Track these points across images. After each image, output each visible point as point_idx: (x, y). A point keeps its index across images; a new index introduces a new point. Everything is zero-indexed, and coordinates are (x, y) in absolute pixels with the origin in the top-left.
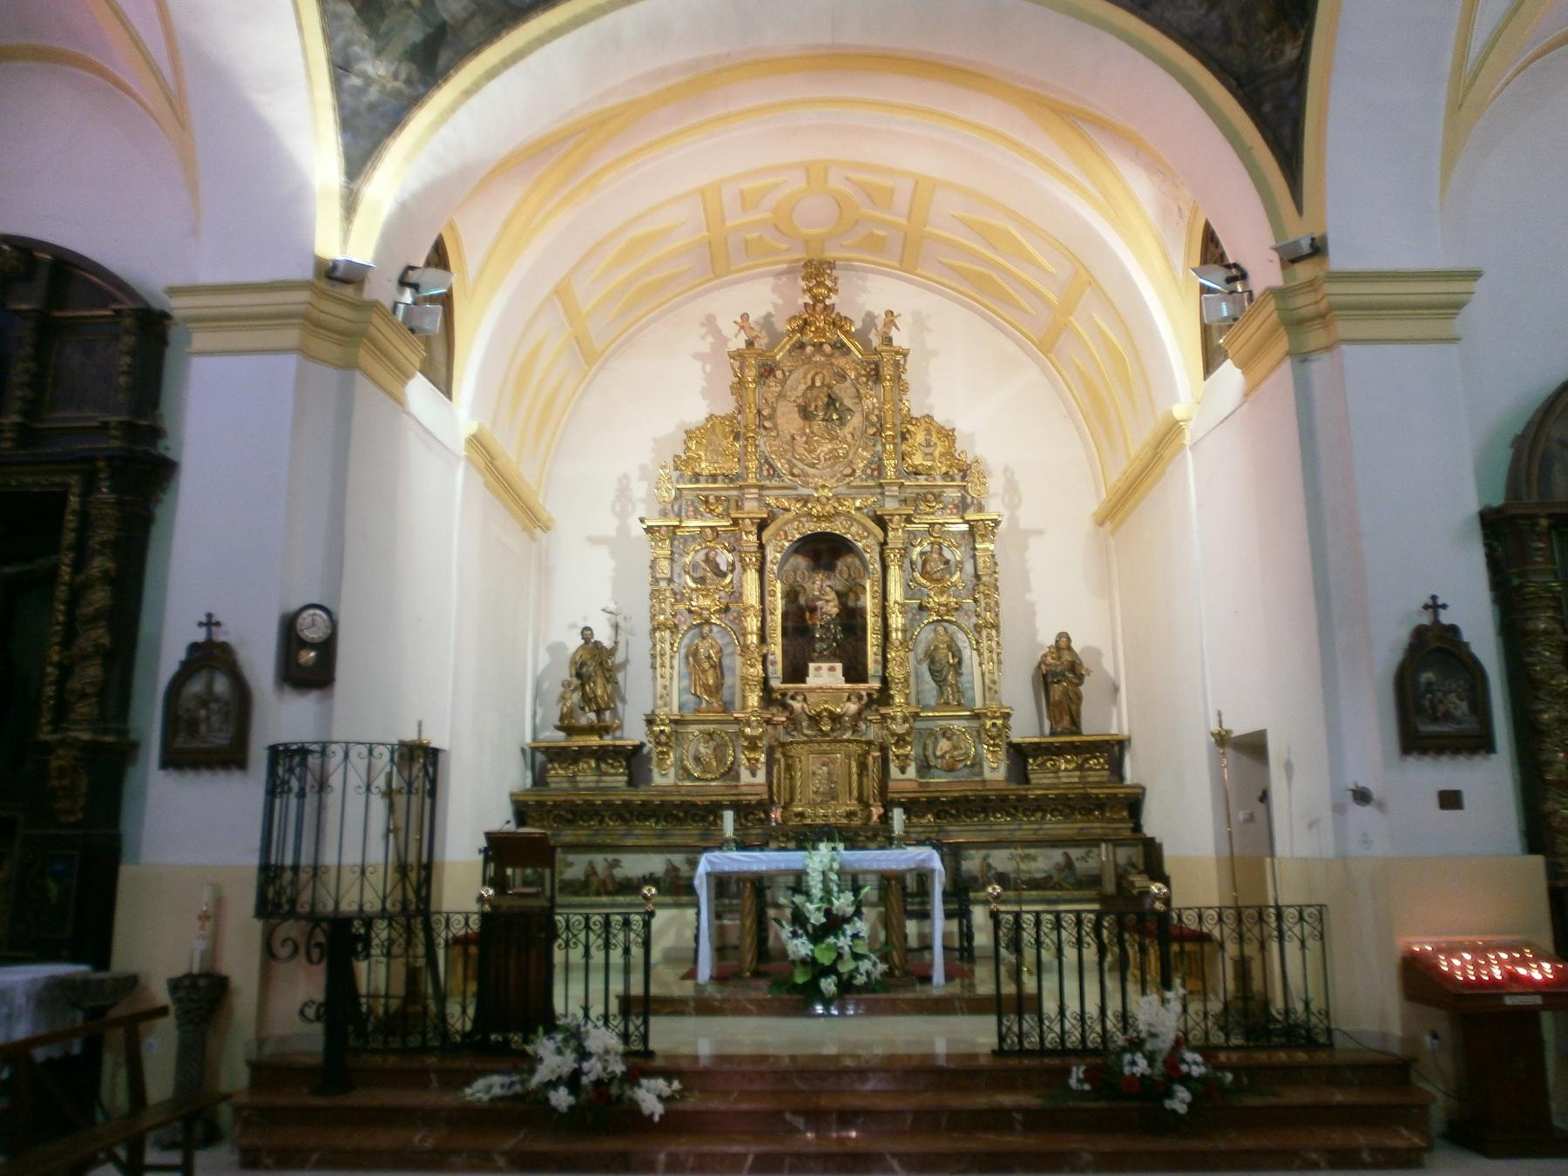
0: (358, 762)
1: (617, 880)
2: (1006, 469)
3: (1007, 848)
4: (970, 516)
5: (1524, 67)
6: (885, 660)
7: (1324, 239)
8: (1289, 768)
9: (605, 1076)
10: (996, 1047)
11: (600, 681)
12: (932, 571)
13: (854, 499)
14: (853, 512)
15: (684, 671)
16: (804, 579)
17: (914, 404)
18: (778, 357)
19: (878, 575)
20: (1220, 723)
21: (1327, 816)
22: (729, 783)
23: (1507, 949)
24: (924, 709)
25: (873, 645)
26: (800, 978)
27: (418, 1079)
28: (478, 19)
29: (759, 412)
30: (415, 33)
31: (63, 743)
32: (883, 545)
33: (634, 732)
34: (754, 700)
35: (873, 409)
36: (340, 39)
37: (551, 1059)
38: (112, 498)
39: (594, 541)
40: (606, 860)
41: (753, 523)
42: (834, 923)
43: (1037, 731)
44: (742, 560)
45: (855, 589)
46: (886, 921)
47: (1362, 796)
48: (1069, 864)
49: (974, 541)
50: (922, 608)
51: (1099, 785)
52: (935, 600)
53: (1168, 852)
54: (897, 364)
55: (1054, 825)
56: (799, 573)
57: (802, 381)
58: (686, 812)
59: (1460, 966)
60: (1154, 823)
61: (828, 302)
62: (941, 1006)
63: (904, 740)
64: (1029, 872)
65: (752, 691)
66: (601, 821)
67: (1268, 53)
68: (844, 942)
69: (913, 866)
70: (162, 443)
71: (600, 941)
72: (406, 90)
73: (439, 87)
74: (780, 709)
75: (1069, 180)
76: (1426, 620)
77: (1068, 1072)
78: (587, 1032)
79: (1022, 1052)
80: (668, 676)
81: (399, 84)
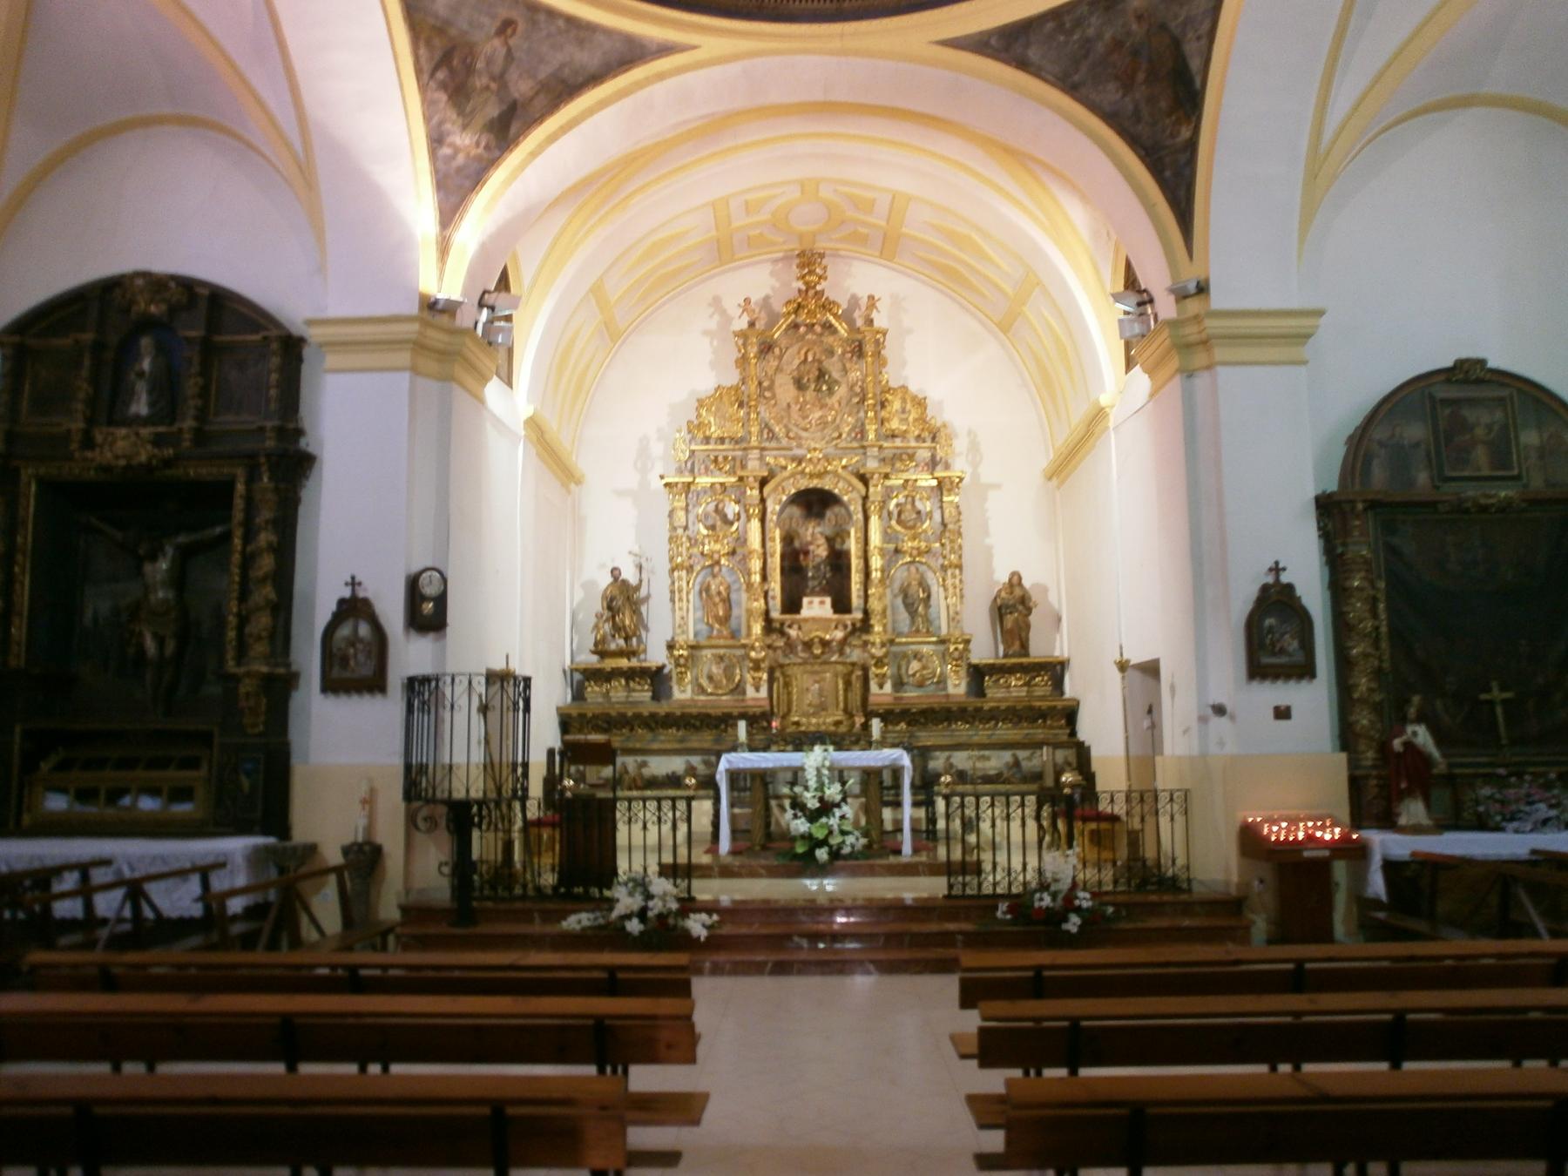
0: (461, 688)
1: (646, 777)
2: (970, 432)
3: (967, 749)
4: (940, 473)
5: (1370, 141)
6: (866, 597)
7: (1207, 281)
8: (1173, 688)
9: (665, 911)
10: (946, 892)
11: (627, 613)
12: (908, 519)
13: (841, 459)
14: (840, 470)
15: (698, 604)
16: (798, 525)
17: (891, 376)
18: (776, 336)
19: (861, 523)
20: (1121, 655)
21: (1194, 724)
22: (736, 697)
23: (1315, 819)
24: (900, 635)
25: (856, 583)
26: (800, 849)
27: (526, 916)
28: (542, 96)
29: (760, 384)
30: (493, 110)
31: (248, 674)
32: (865, 498)
33: (656, 655)
34: (757, 629)
35: (857, 381)
36: (435, 120)
37: (625, 901)
38: (271, 485)
39: (620, 493)
40: (636, 761)
41: (756, 481)
42: (826, 808)
43: (993, 654)
44: (747, 511)
45: (840, 535)
46: (867, 809)
47: (1220, 710)
48: (1017, 763)
49: (942, 494)
50: (897, 551)
51: (1042, 698)
52: (908, 545)
53: (1094, 753)
54: (877, 342)
55: (1005, 732)
56: (794, 520)
57: (797, 357)
58: (702, 722)
59: (1276, 832)
60: (1085, 732)
61: (819, 288)
62: (909, 870)
63: (882, 662)
64: (984, 769)
65: (756, 622)
66: (632, 729)
67: (1168, 132)
68: (834, 822)
69: (887, 763)
70: (303, 443)
71: (655, 819)
72: (486, 155)
73: (511, 151)
74: (779, 636)
75: (1018, 203)
76: (1270, 579)
77: (996, 908)
78: (650, 882)
79: (964, 897)
80: (685, 608)
81: (480, 150)
